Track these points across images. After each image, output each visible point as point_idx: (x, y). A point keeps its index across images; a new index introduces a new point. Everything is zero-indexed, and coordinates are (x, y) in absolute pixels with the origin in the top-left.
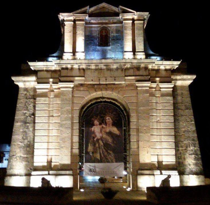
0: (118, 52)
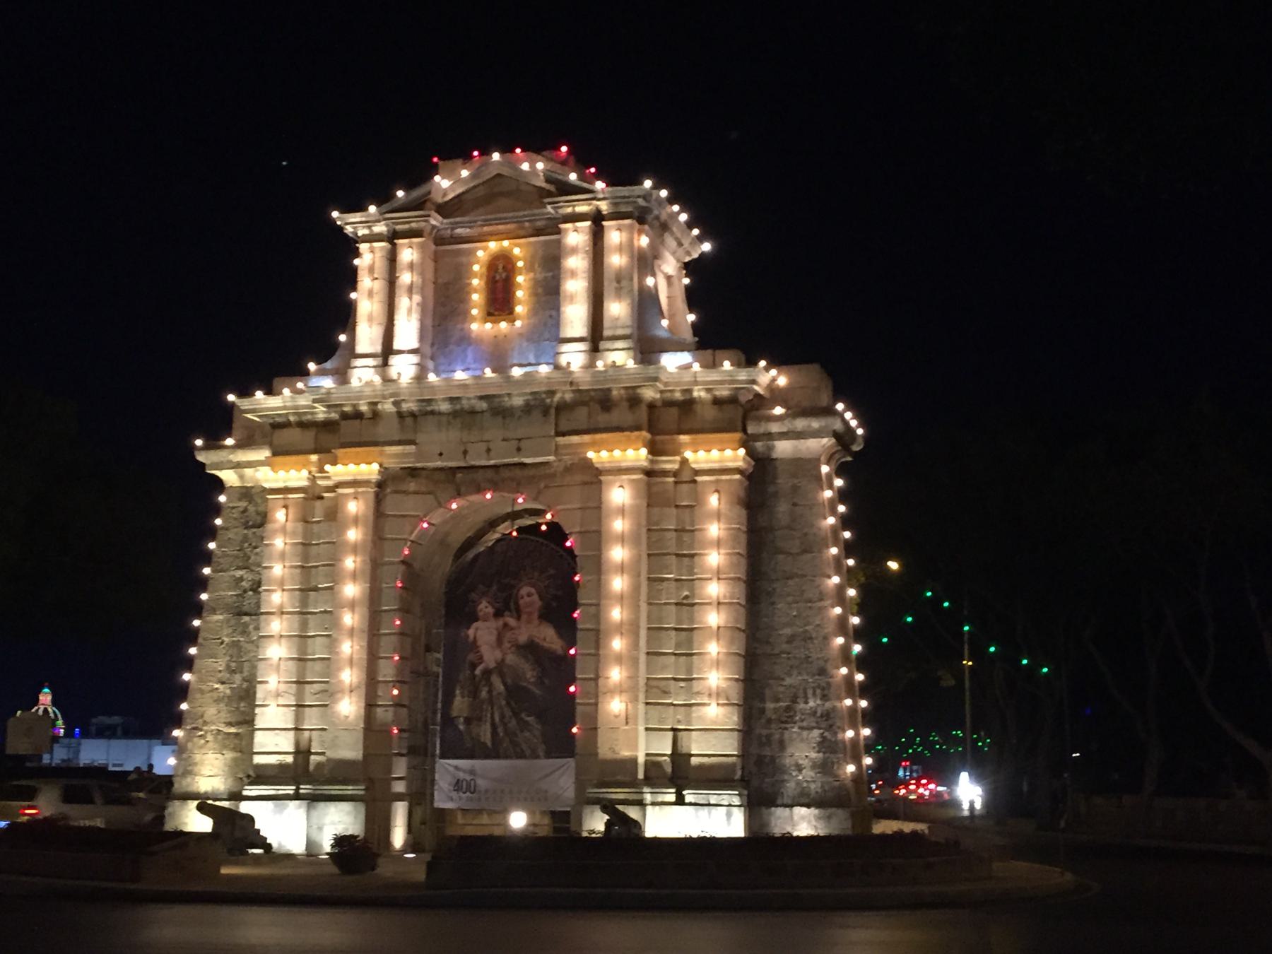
0: (548, 340)
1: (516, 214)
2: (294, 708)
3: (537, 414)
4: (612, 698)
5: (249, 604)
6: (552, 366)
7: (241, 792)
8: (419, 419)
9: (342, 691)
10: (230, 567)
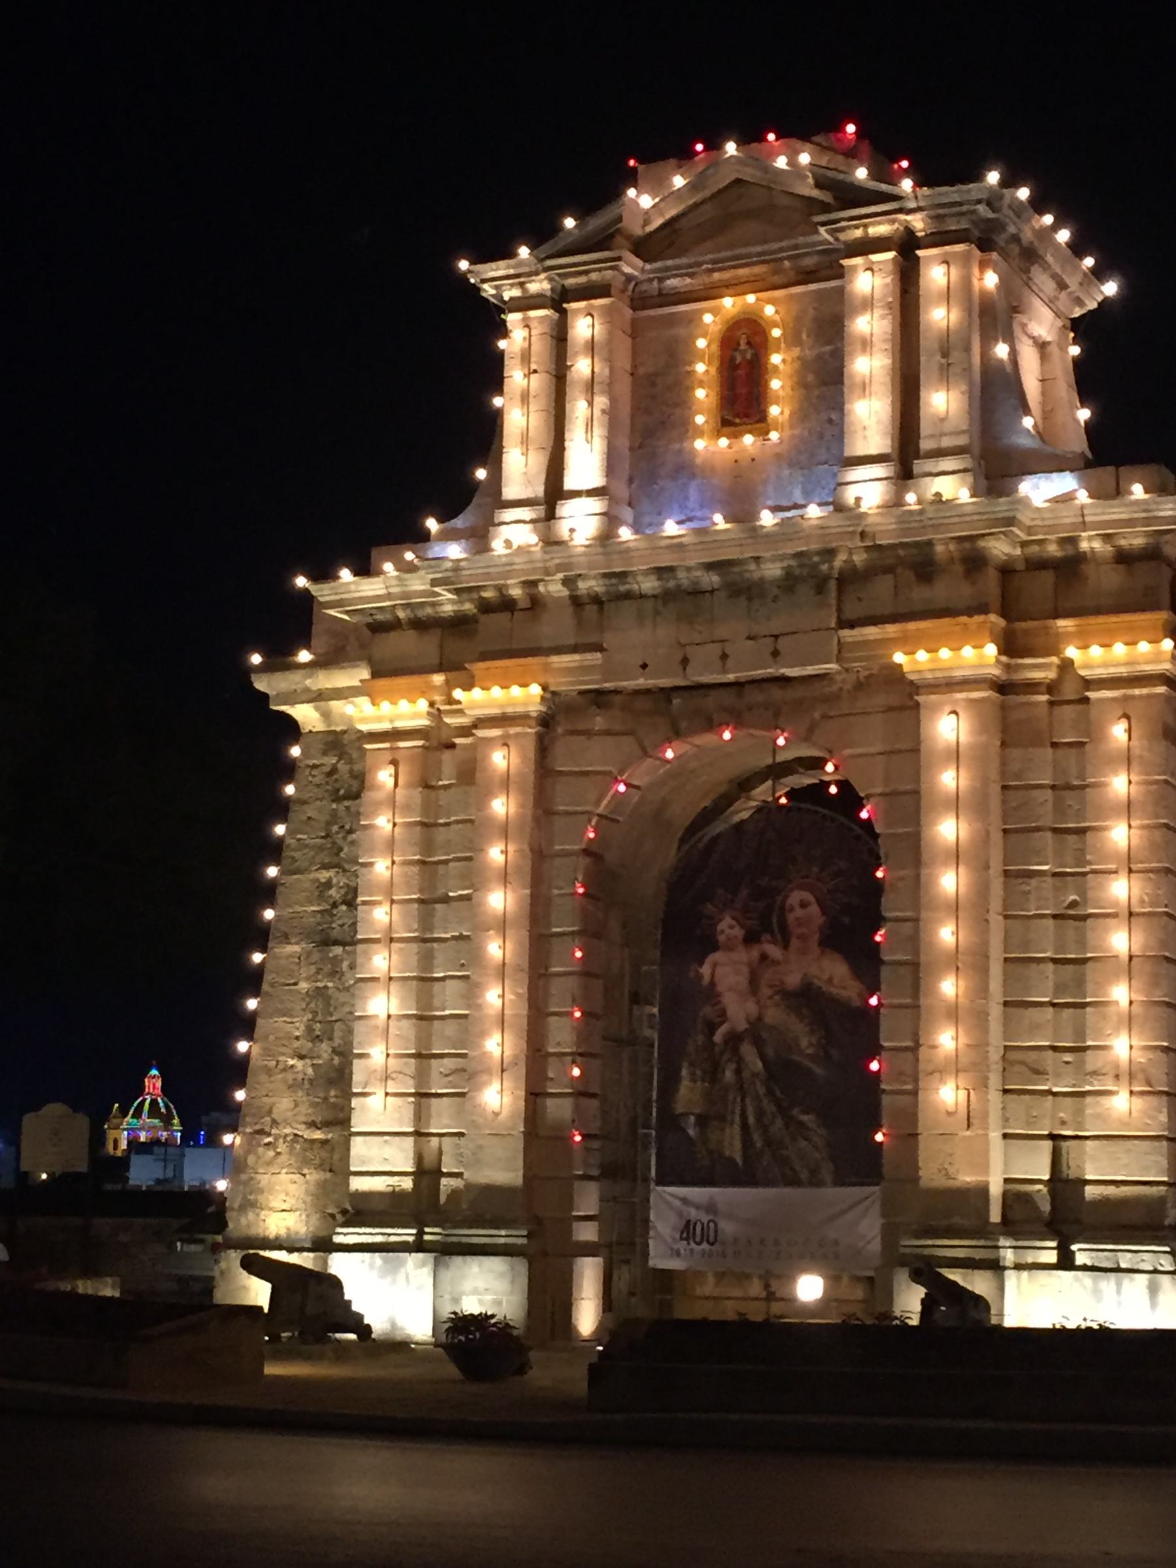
1: (766, 247)
2: (412, 1099)
3: (805, 591)
4: (942, 1081)
5: (342, 926)
6: (831, 508)
7: (331, 1239)
8: (606, 607)
9: (488, 1071)
10: (312, 864)
